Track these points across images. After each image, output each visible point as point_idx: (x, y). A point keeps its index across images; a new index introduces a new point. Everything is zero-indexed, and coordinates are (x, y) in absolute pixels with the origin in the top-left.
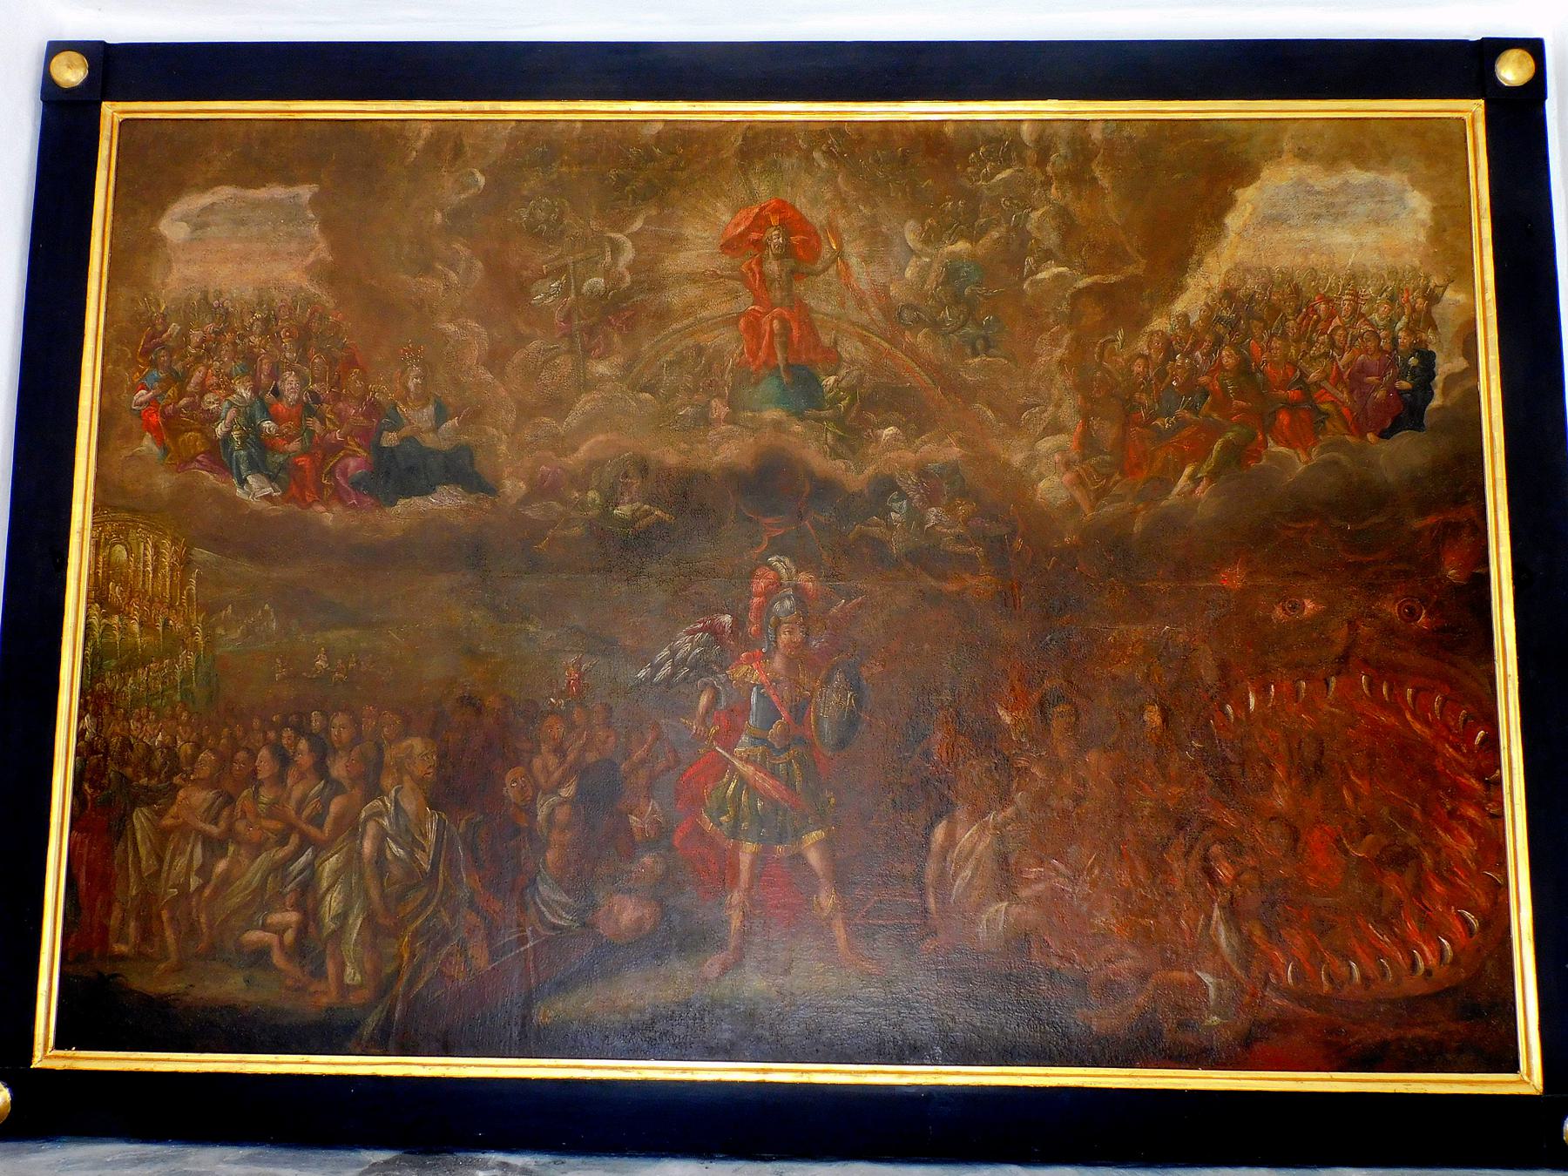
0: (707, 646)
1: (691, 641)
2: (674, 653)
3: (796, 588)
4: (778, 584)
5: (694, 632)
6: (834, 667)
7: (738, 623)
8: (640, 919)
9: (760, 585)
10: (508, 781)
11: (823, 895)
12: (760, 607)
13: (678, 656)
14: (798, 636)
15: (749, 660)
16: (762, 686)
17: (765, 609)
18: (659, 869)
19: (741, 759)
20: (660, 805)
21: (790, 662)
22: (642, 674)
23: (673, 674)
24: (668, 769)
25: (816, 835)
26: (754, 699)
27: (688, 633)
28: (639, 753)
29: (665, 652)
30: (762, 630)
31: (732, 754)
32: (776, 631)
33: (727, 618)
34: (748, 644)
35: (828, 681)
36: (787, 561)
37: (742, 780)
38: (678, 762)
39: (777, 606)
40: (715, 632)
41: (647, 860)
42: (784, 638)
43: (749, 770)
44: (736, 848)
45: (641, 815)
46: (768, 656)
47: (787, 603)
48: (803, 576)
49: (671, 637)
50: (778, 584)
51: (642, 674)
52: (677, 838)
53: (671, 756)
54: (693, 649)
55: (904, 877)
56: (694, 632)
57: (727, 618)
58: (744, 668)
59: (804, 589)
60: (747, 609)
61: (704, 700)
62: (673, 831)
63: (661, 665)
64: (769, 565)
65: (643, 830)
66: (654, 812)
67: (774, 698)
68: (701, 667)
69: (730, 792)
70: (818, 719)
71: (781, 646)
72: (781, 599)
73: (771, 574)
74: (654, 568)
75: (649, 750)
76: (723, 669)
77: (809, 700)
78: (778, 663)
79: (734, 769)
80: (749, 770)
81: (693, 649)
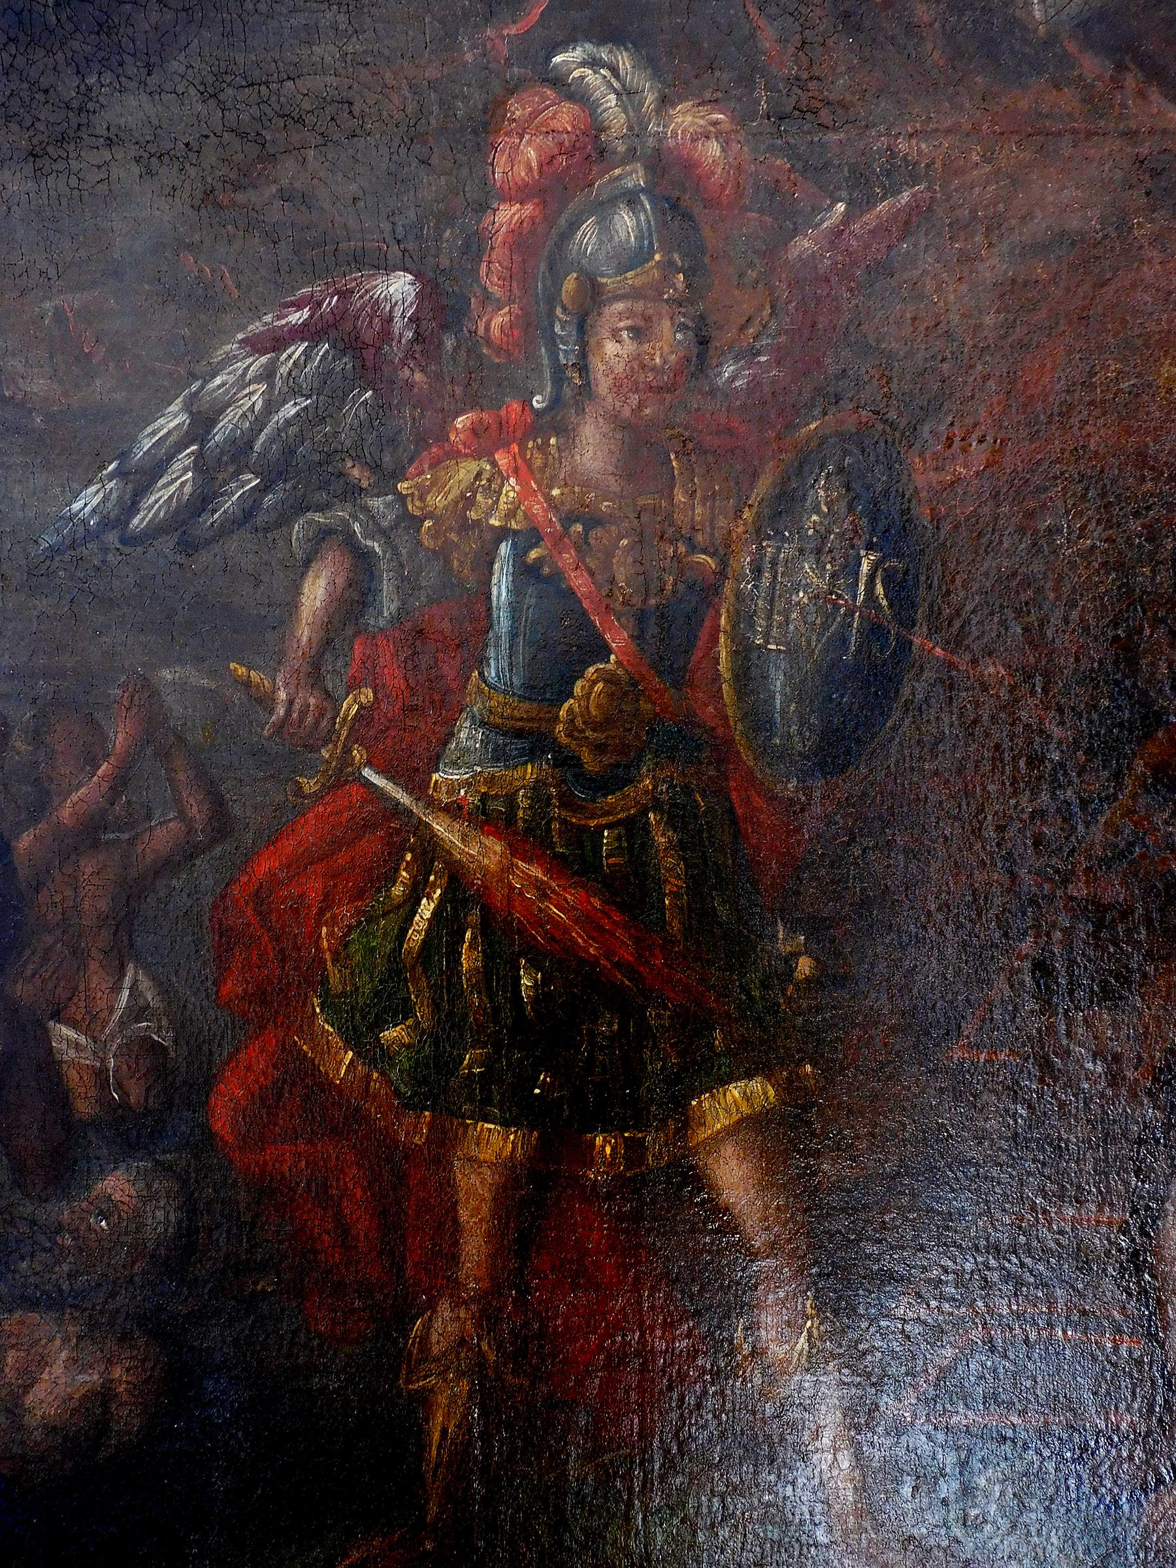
0: (329, 392)
1: (268, 374)
2: (202, 422)
3: (660, 163)
4: (590, 150)
5: (277, 342)
6: (805, 462)
7: (442, 306)
8: (104, 1395)
9: (521, 157)
10: (489, 841)
11: (770, 1324)
12: (522, 241)
13: (220, 433)
14: (669, 342)
15: (484, 442)
16: (533, 536)
17: (541, 248)
18: (161, 1219)
19: (454, 811)
20: (164, 988)
21: (640, 448)
22: (88, 501)
23: (203, 501)
24: (188, 853)
25: (739, 1097)
26: (501, 589)
27: (255, 345)
28: (80, 797)
29: (173, 419)
30: (533, 326)
31: (417, 784)
32: (583, 326)
33: (399, 288)
34: (480, 381)
35: (785, 504)
36: (624, 61)
37: (460, 889)
38: (222, 824)
39: (587, 235)
40: (354, 340)
41: (117, 1185)
42: (613, 352)
43: (482, 852)
44: (443, 1144)
45: (89, 1024)
46: (556, 423)
47: (626, 223)
48: (685, 119)
49: (194, 361)
50: (590, 150)
51: (88, 501)
52: (225, 1110)
53: (197, 810)
54: (271, 406)
55: (1082, 1257)
56: (277, 342)
57: (399, 288)
58: (465, 471)
59: (689, 165)
60: (475, 246)
61: (316, 592)
62: (208, 1083)
63: (156, 468)
64: (558, 82)
65: (100, 1075)
66: (138, 1011)
67: (579, 582)
68: (307, 472)
69: (416, 935)
70: (744, 652)
71: (603, 385)
72: (603, 208)
73: (565, 116)
74: (130, 110)
75: (120, 783)
76: (387, 478)
77: (706, 592)
78: (592, 449)
79: (430, 851)
80: (482, 852)
81: (271, 406)
